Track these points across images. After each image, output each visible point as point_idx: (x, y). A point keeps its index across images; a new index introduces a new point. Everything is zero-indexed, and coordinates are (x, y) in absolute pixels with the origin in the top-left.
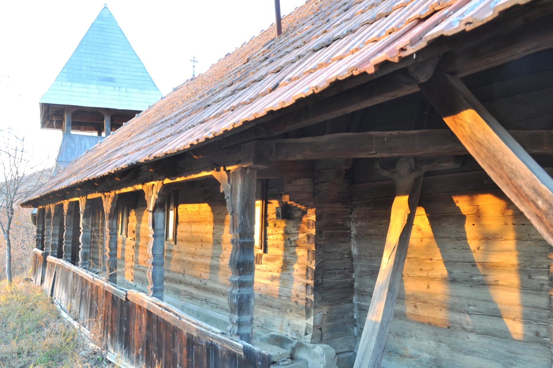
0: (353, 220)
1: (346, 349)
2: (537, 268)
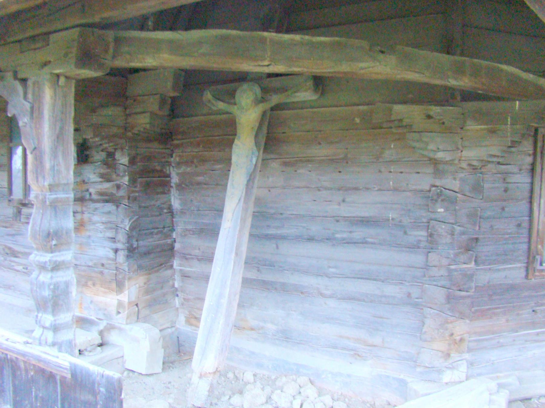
0: (173, 165)
1: (168, 325)
2: (415, 222)
